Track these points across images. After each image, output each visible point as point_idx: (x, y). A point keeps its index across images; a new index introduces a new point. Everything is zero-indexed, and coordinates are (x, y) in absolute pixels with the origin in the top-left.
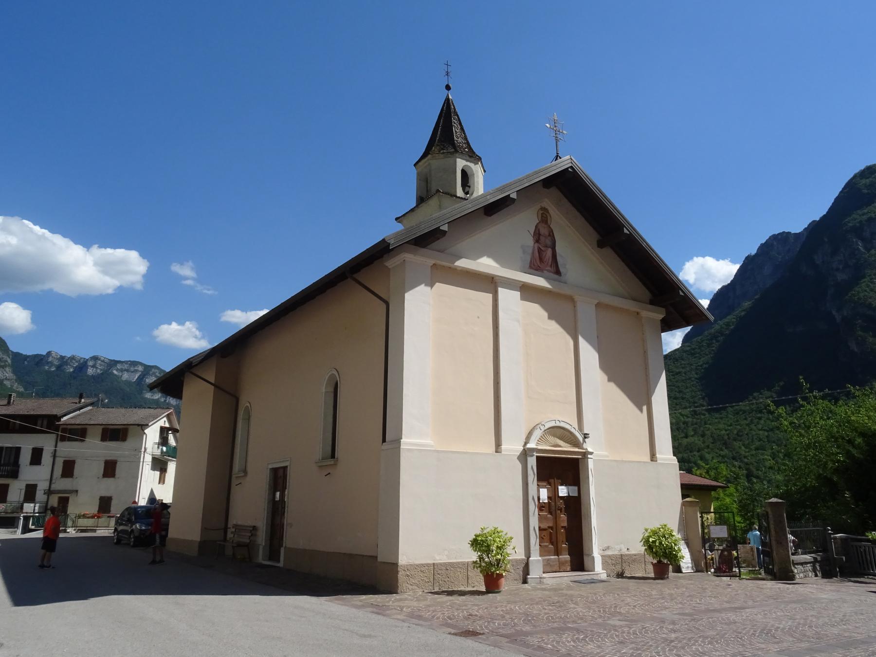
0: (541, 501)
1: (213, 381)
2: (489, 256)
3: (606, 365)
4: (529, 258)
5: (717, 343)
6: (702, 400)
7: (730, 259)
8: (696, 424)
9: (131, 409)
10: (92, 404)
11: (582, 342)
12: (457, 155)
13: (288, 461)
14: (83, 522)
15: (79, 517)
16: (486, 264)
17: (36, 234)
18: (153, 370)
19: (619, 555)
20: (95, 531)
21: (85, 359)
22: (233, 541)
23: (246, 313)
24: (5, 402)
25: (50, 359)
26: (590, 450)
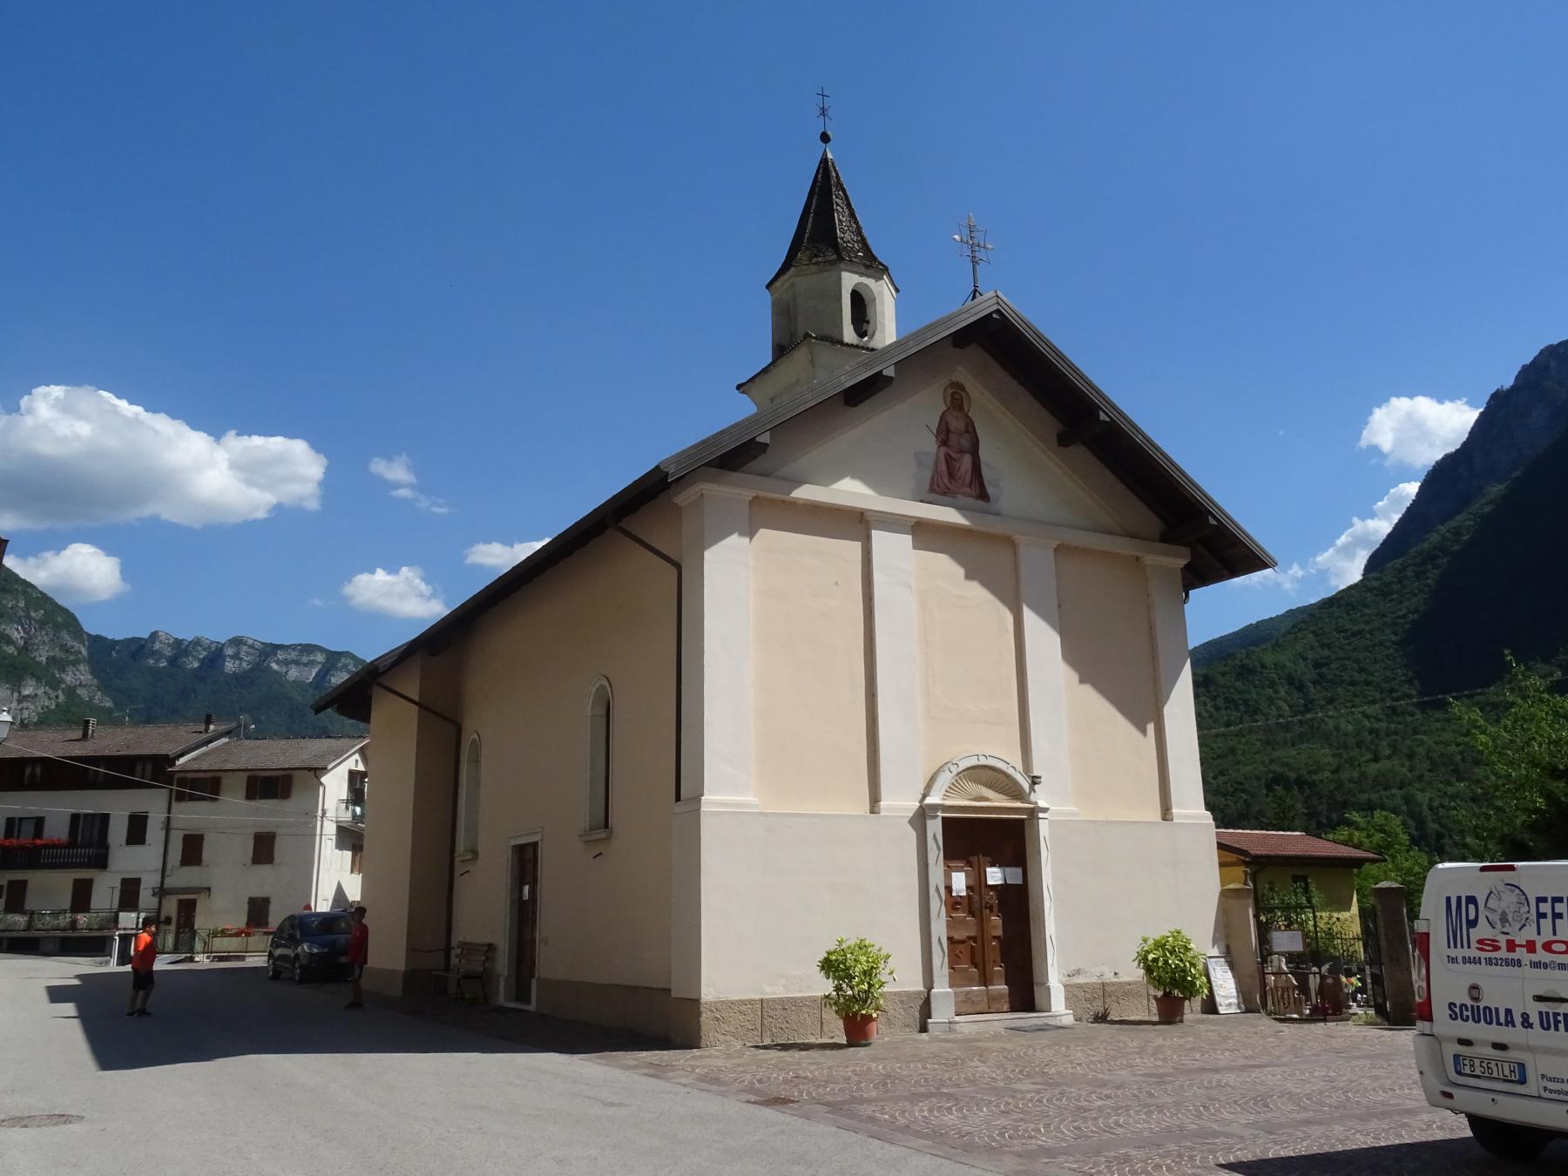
0: (954, 894)
1: (416, 698)
2: (854, 477)
3: (1081, 656)
4: (928, 474)
5: (1435, 571)
6: (1406, 686)
7: (1465, 399)
8: (1395, 733)
9: (296, 740)
10: (228, 733)
11: (1029, 615)
12: (842, 266)
13: (538, 832)
14: (221, 944)
15: (215, 934)
16: (850, 491)
17: (124, 417)
18: (343, 660)
19: (1098, 984)
20: (242, 958)
21: (218, 643)
22: (458, 970)
23: (512, 546)
24: (78, 734)
25: (157, 646)
26: (1042, 804)
